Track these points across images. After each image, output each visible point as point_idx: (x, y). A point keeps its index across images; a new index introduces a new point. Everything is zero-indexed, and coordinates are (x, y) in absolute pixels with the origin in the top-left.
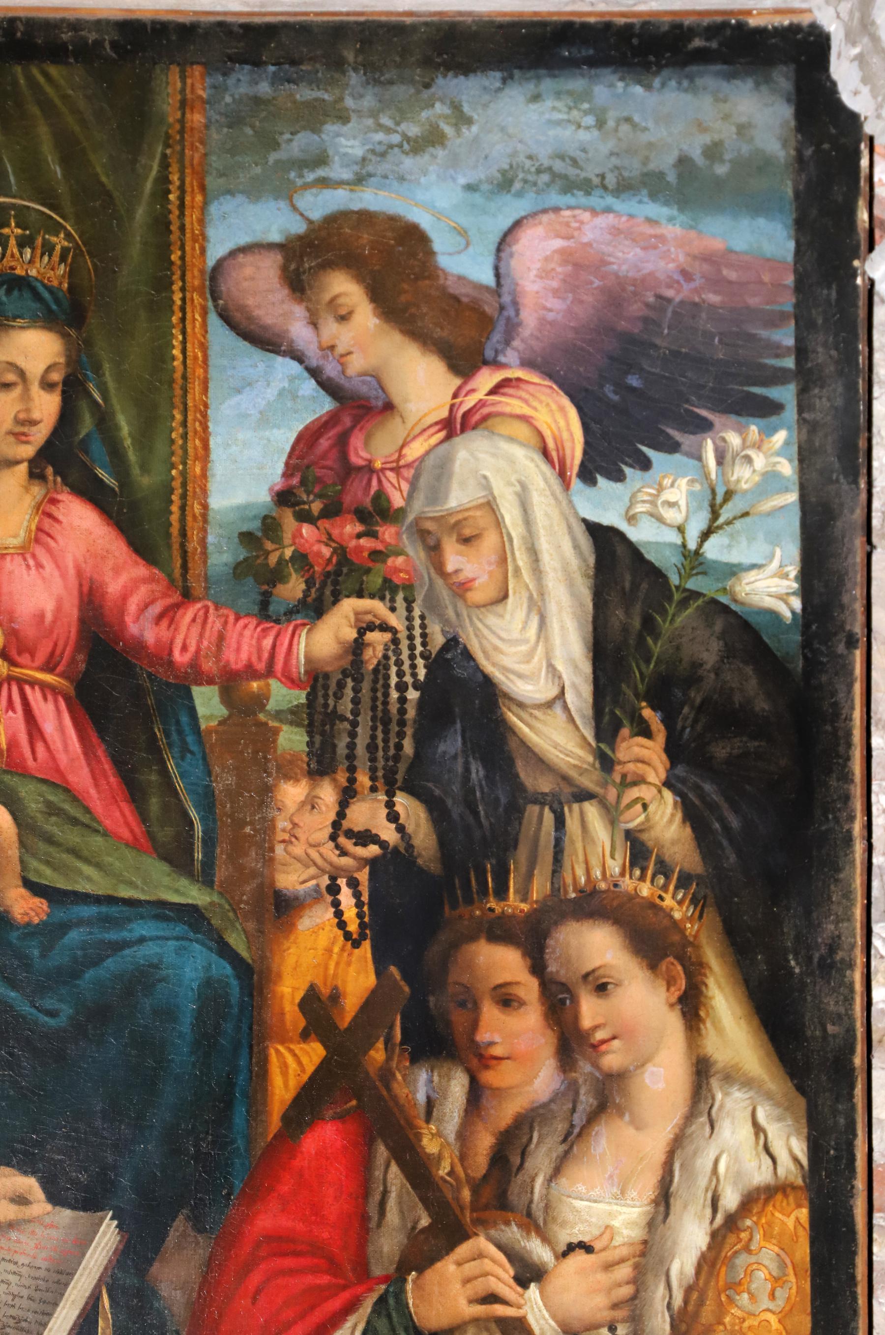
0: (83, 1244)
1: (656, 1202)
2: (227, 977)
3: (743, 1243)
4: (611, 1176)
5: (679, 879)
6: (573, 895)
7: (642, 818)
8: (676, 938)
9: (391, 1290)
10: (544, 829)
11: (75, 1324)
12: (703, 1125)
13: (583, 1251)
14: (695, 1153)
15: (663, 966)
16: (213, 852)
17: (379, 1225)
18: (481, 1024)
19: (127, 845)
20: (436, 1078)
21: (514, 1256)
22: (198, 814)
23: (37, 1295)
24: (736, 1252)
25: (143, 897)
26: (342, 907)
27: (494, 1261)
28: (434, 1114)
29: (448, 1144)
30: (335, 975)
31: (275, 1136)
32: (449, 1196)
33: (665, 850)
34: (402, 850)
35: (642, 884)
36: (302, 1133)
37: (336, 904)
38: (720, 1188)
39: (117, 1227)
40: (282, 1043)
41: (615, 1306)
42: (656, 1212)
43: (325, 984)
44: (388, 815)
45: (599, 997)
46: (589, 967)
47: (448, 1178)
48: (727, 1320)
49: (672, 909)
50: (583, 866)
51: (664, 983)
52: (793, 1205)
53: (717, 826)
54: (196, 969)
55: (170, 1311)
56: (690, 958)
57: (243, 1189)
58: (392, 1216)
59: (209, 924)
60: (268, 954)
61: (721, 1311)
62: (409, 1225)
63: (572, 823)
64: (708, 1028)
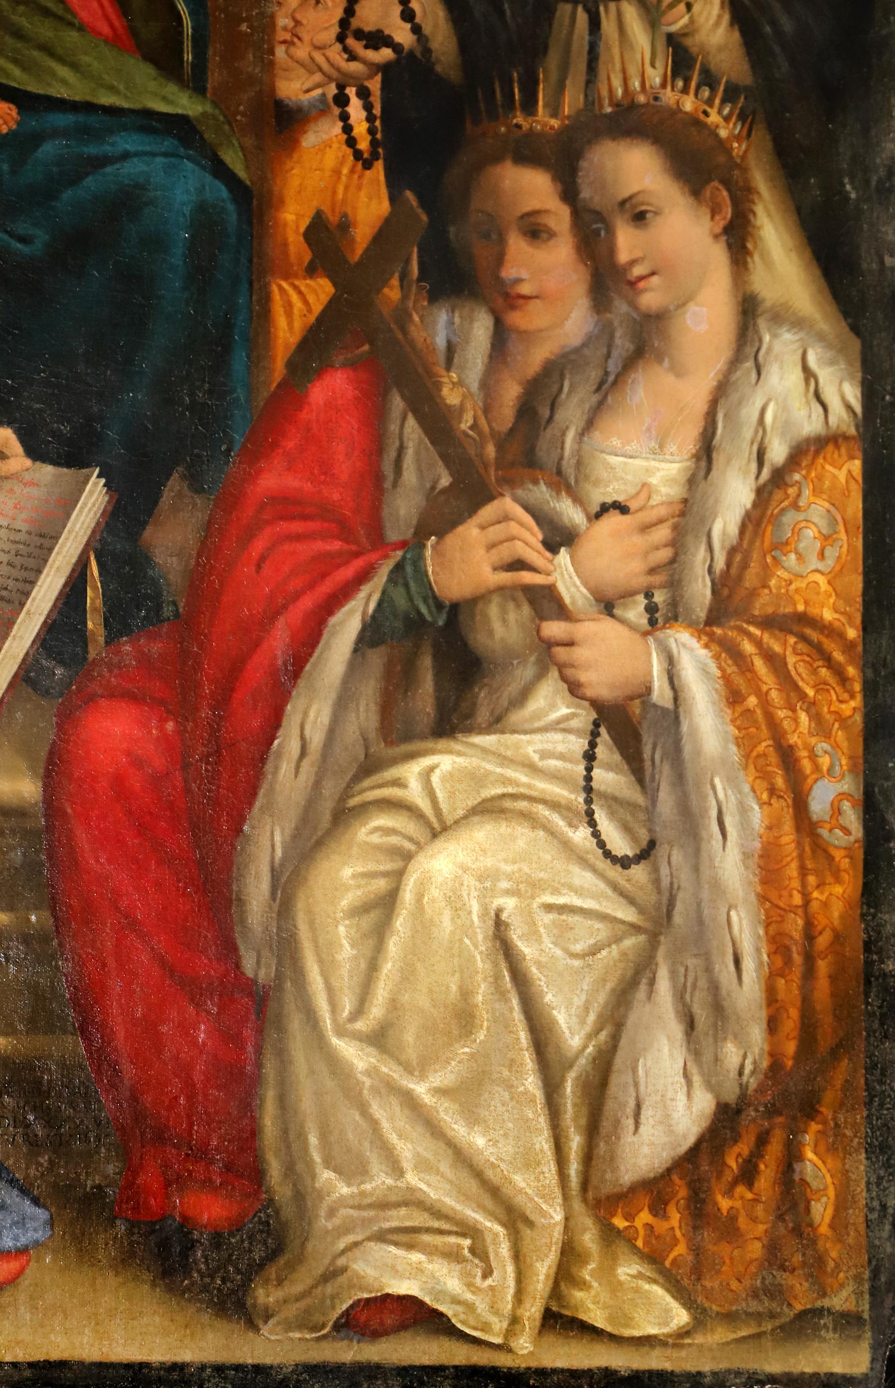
0: (68, 504)
1: (697, 457)
2: (223, 200)
3: (791, 499)
4: (649, 429)
5: (725, 90)
6: (609, 110)
7: (685, 20)
8: (722, 159)
9: (408, 556)
10: (577, 31)
11: (61, 593)
12: (749, 371)
13: (617, 511)
14: (740, 403)
15: (707, 192)
16: (205, 53)
17: (395, 485)
18: (507, 257)
19: (107, 41)
20: (457, 320)
21: (542, 518)
22: (188, 8)
23: (18, 561)
24: (783, 510)
25: (126, 105)
26: (352, 121)
27: (521, 524)
28: (455, 360)
29: (471, 394)
30: (344, 201)
31: (279, 386)
32: (472, 452)
33: (711, 58)
34: (418, 54)
35: (685, 97)
36: (309, 381)
37: (345, 117)
38: (766, 441)
39: (105, 485)
40: (286, 278)
41: (652, 571)
42: (697, 468)
43: (333, 211)
44: (402, 12)
45: (637, 227)
46: (626, 194)
47: (471, 433)
48: (773, 582)
49: (717, 126)
50: (620, 76)
51: (708, 211)
52: (845, 458)
53: (768, 29)
54: (188, 192)
55: (165, 579)
56: (737, 182)
57: (244, 444)
58: (410, 475)
59: (202, 138)
60: (269, 176)
61: (766, 572)
62: (428, 485)
63: (608, 26)
64: (756, 262)
